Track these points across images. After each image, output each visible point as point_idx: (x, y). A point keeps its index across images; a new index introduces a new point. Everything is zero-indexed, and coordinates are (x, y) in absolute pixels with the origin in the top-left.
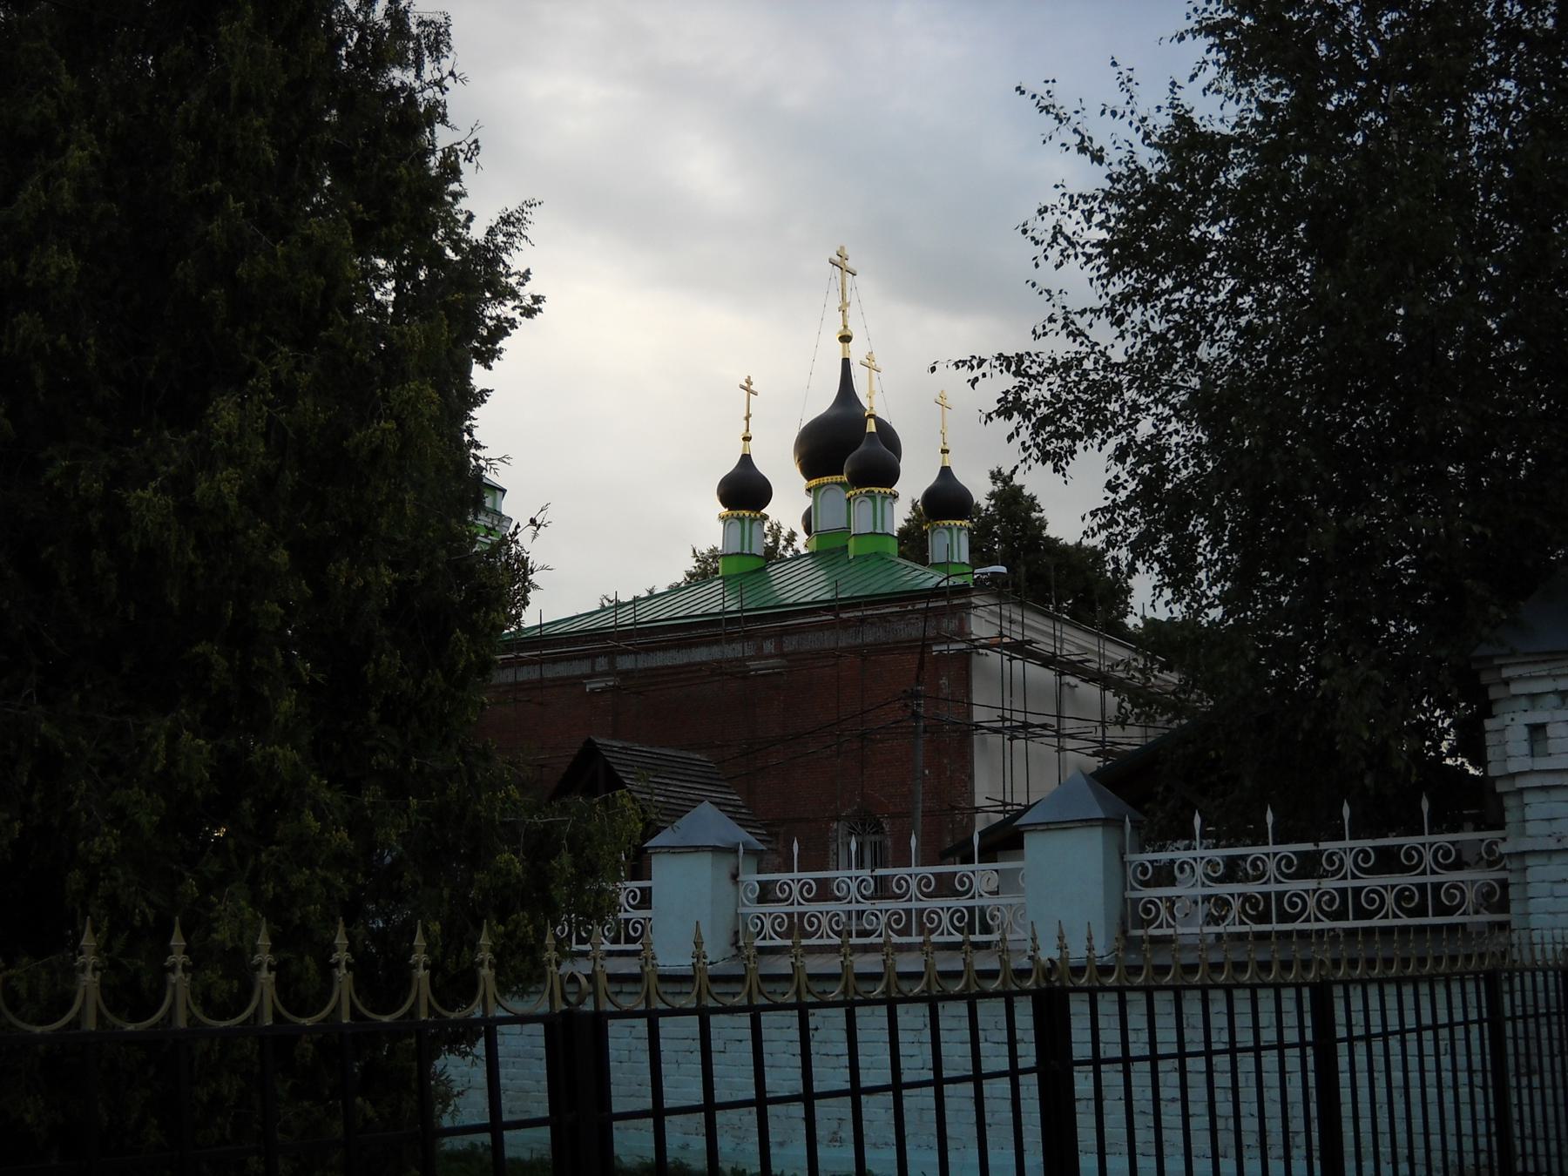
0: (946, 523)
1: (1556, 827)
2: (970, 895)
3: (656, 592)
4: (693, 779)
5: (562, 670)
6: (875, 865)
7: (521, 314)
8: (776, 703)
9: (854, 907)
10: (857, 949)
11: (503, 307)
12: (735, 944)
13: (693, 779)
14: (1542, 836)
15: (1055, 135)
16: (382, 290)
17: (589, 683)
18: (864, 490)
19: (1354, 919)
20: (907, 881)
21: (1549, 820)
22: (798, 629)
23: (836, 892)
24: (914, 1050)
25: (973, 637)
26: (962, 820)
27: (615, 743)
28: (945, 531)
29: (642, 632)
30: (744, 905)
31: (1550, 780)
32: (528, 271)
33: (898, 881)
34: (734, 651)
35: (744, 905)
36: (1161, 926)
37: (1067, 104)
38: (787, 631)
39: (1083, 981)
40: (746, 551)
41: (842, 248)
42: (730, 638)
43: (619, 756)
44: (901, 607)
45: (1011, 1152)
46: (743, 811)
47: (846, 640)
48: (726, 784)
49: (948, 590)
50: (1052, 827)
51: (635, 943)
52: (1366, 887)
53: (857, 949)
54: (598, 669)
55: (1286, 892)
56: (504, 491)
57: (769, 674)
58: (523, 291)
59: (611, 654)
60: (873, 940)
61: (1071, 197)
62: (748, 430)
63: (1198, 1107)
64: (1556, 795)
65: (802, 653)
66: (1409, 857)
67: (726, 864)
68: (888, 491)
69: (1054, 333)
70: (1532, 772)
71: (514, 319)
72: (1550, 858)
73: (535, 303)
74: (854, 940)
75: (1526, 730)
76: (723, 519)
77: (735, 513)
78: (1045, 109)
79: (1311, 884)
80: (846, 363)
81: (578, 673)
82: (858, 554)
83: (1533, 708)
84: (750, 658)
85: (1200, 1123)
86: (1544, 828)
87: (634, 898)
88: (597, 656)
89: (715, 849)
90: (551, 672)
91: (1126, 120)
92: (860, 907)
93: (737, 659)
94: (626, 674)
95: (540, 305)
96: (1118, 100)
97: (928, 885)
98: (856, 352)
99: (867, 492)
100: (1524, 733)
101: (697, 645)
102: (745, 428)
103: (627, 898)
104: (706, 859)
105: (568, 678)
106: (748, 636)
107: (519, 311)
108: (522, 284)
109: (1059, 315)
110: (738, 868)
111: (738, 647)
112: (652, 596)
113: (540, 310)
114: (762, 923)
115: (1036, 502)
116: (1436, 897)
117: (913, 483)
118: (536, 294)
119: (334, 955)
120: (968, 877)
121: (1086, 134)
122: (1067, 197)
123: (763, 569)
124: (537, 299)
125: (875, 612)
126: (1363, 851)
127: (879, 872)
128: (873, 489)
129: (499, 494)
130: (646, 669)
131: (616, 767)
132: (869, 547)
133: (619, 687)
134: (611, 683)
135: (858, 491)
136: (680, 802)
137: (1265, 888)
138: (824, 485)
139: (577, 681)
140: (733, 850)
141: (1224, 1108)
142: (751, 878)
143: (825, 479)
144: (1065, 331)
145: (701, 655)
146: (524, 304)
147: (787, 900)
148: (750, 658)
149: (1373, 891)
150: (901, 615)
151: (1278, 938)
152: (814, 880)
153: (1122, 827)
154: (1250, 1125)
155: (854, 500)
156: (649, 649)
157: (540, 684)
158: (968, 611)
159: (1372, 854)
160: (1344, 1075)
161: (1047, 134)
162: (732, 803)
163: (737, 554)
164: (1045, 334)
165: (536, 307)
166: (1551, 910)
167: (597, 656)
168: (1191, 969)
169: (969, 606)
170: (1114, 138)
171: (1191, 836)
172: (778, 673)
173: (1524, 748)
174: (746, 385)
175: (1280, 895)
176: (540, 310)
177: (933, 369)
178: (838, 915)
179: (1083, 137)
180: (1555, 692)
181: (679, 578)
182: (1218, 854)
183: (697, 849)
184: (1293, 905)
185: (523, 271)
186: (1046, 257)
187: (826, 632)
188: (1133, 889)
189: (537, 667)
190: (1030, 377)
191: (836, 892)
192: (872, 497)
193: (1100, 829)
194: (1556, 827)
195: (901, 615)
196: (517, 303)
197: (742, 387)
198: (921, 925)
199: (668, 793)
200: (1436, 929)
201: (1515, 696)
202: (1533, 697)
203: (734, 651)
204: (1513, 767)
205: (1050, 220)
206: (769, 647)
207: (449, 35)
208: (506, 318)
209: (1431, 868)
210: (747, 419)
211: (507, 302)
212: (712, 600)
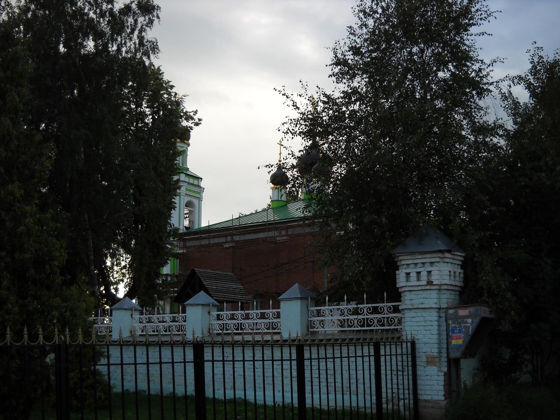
1: (413, 302)
3: (258, 211)
4: (227, 281)
5: (216, 241)
6: (261, 309)
7: (194, 125)
9: (255, 321)
10: (256, 333)
11: (188, 123)
12: (209, 332)
13: (227, 281)
14: (409, 304)
15: (286, 102)
16: (148, 118)
19: (367, 327)
21: (411, 300)
27: (201, 270)
29: (242, 228)
30: (212, 321)
31: (411, 289)
32: (197, 111)
34: (271, 234)
35: (212, 321)
37: (289, 93)
39: (287, 343)
42: (270, 230)
43: (202, 274)
45: (294, 396)
46: (243, 291)
47: (307, 230)
48: (239, 282)
50: (284, 300)
51: (371, 327)
53: (236, 334)
54: (228, 240)
56: (201, 179)
58: (195, 117)
59: (232, 235)
60: (260, 331)
61: (291, 120)
62: (280, 158)
63: (323, 380)
64: (413, 293)
66: (381, 309)
67: (207, 309)
69: (289, 158)
70: (406, 286)
71: (192, 127)
72: (411, 310)
73: (199, 121)
74: (255, 331)
75: (405, 274)
76: (272, 188)
77: (276, 186)
78: (284, 95)
79: (355, 317)
81: (221, 241)
83: (408, 268)
84: (277, 237)
85: (323, 384)
86: (409, 302)
87: (370, 310)
88: (228, 236)
89: (202, 305)
90: (213, 241)
91: (304, 97)
93: (273, 237)
94: (237, 242)
95: (201, 122)
96: (302, 91)
100: (404, 275)
101: (260, 232)
102: (279, 158)
104: (200, 308)
105: (218, 243)
106: (277, 229)
107: (193, 124)
108: (195, 115)
109: (291, 153)
110: (210, 310)
111: (273, 232)
112: (257, 212)
113: (201, 123)
114: (262, 325)
116: (388, 321)
118: (199, 118)
120: (343, 310)
121: (295, 101)
122: (290, 120)
123: (286, 205)
124: (200, 120)
126: (369, 307)
127: (246, 312)
129: (200, 180)
130: (243, 240)
131: (200, 278)
133: (233, 246)
134: (231, 245)
136: (222, 288)
137: (344, 318)
140: (209, 305)
141: (331, 380)
142: (215, 313)
144: (293, 158)
145: (261, 235)
146: (195, 122)
147: (253, 318)
148: (277, 237)
149: (352, 320)
151: (363, 332)
153: (308, 300)
154: (339, 385)
156: (244, 234)
157: (209, 245)
159: (392, 308)
160: (383, 371)
161: (284, 102)
162: (240, 288)
163: (277, 200)
164: (287, 159)
165: (199, 122)
166: (410, 325)
167: (228, 236)
168: (322, 340)
171: (325, 302)
172: (287, 241)
173: (404, 279)
174: (280, 143)
175: (367, 319)
176: (201, 123)
177: (259, 168)
179: (294, 102)
180: (413, 263)
181: (266, 206)
182: (259, 311)
183: (198, 305)
184: (371, 322)
185: (195, 110)
186: (285, 138)
188: (311, 317)
189: (208, 239)
190: (287, 169)
193: (300, 300)
194: (413, 302)
196: (192, 121)
197: (278, 144)
198: (182, 330)
199: (217, 286)
200: (366, 331)
201: (403, 264)
202: (408, 265)
203: (271, 234)
204: (401, 285)
205: (286, 126)
206: (283, 233)
207: (158, 46)
208: (189, 126)
210: (280, 154)
211: (189, 121)
212: (271, 217)
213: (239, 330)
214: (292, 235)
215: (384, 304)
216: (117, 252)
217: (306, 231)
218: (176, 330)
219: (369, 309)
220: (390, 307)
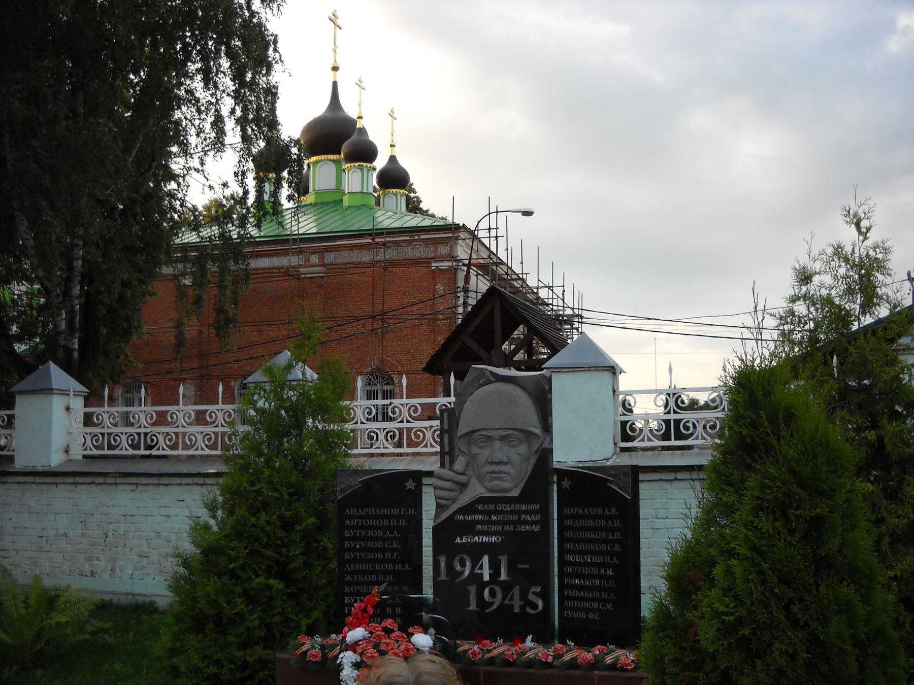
0: (394, 190)
2: (102, 426)
8: (319, 296)
18: (357, 164)
20: (215, 414)
22: (337, 249)
23: (132, 419)
25: (459, 258)
28: (393, 196)
33: (394, 408)
36: (643, 440)
38: (327, 249)
41: (335, 11)
44: (410, 236)
49: (453, 227)
51: (417, 447)
52: (683, 419)
55: (628, 421)
57: (315, 277)
65: (338, 264)
68: (369, 165)
80: (335, 84)
82: (351, 205)
84: (300, 266)
92: (147, 430)
97: (416, 411)
98: (340, 76)
103: (224, 418)
106: (300, 252)
115: (413, 187)
117: (380, 163)
125: (391, 240)
128: (362, 163)
132: (358, 201)
135: (352, 165)
138: (322, 160)
143: (323, 157)
150: (409, 242)
152: (155, 412)
155: (349, 171)
158: (456, 242)
169: (457, 238)
178: (133, 435)
184: (417, 436)
187: (355, 251)
191: (132, 419)
192: (361, 168)
195: (409, 242)
203: (294, 260)
206: (314, 259)
209: (674, 410)
213: (103, 449)
214: (334, 265)
215: (216, 407)
216: (188, 282)
217: (364, 259)
218: (206, 446)
219: (413, 408)
220: (416, 407)
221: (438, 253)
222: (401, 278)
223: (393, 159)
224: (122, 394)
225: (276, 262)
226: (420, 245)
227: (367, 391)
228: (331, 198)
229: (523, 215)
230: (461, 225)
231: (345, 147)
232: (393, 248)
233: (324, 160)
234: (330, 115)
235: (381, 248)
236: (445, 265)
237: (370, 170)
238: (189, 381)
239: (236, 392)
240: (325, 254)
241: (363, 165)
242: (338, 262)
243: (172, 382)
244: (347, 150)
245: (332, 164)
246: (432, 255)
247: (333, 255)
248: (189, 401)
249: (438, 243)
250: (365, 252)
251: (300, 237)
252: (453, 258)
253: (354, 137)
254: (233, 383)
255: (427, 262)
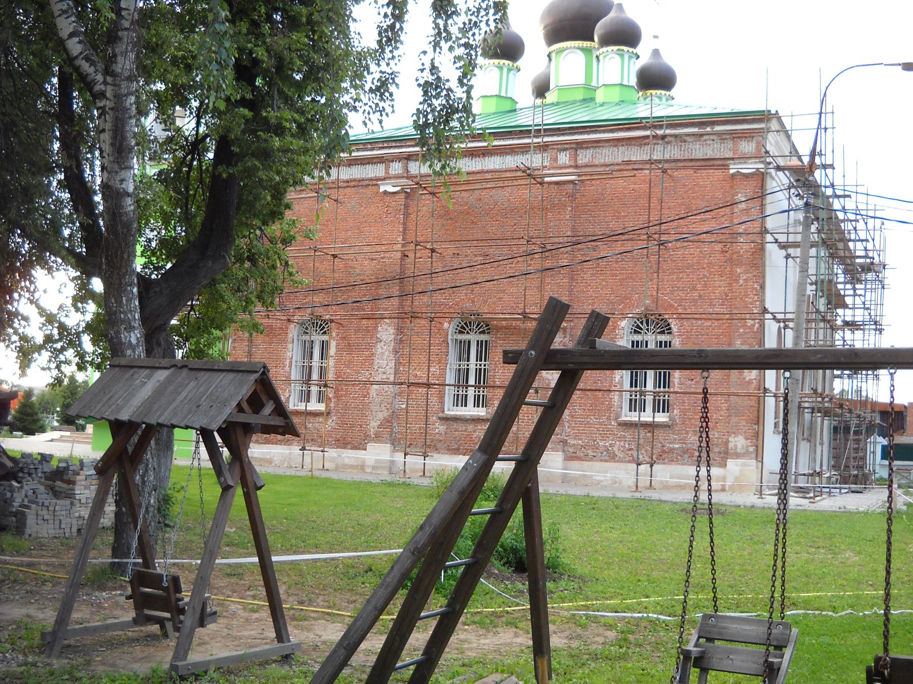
0: (659, 92)
8: (569, 209)
17: (383, 184)
24: (702, 553)
26: (753, 325)
38: (580, 145)
40: (503, 94)
54: (392, 172)
68: (631, 50)
81: (371, 175)
99: (619, 50)
117: (644, 50)
119: (114, 508)
139: (374, 182)
170: (402, 55)
203: (535, 160)
206: (564, 158)
221: (740, 151)
222: (684, 185)
223: (656, 52)
224: (298, 336)
225: (511, 161)
226: (713, 140)
227: (478, 341)
228: (579, 95)
229: (904, 69)
230: (773, 112)
231: (599, 30)
232: (674, 143)
233: (571, 47)
234: (651, 61)
235: (658, 144)
236: (749, 168)
237: (632, 57)
238: (387, 320)
239: (450, 337)
240: (578, 152)
241: (623, 50)
242: (596, 162)
243: (364, 322)
244: (600, 32)
245: (579, 51)
246: (729, 154)
247: (589, 153)
248: (385, 348)
249: (739, 137)
250: (634, 149)
251: (545, 127)
252: (762, 155)
253: (612, 15)
254: (446, 325)
255: (722, 164)
